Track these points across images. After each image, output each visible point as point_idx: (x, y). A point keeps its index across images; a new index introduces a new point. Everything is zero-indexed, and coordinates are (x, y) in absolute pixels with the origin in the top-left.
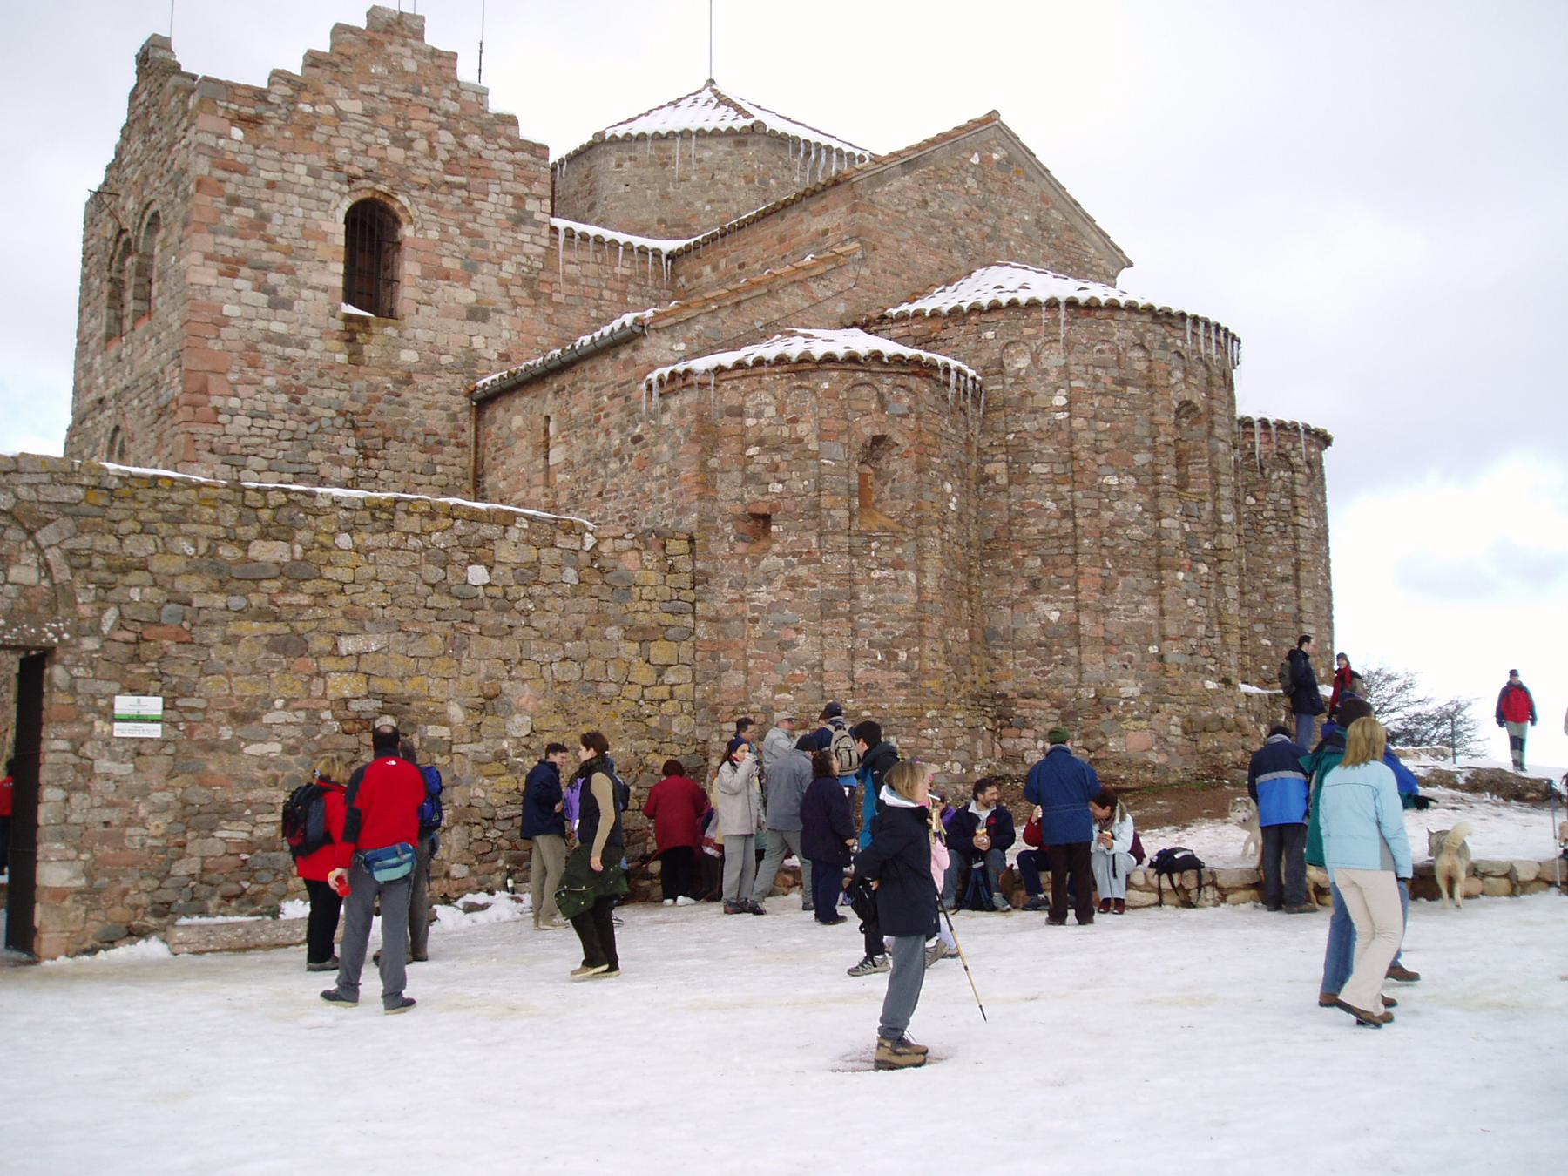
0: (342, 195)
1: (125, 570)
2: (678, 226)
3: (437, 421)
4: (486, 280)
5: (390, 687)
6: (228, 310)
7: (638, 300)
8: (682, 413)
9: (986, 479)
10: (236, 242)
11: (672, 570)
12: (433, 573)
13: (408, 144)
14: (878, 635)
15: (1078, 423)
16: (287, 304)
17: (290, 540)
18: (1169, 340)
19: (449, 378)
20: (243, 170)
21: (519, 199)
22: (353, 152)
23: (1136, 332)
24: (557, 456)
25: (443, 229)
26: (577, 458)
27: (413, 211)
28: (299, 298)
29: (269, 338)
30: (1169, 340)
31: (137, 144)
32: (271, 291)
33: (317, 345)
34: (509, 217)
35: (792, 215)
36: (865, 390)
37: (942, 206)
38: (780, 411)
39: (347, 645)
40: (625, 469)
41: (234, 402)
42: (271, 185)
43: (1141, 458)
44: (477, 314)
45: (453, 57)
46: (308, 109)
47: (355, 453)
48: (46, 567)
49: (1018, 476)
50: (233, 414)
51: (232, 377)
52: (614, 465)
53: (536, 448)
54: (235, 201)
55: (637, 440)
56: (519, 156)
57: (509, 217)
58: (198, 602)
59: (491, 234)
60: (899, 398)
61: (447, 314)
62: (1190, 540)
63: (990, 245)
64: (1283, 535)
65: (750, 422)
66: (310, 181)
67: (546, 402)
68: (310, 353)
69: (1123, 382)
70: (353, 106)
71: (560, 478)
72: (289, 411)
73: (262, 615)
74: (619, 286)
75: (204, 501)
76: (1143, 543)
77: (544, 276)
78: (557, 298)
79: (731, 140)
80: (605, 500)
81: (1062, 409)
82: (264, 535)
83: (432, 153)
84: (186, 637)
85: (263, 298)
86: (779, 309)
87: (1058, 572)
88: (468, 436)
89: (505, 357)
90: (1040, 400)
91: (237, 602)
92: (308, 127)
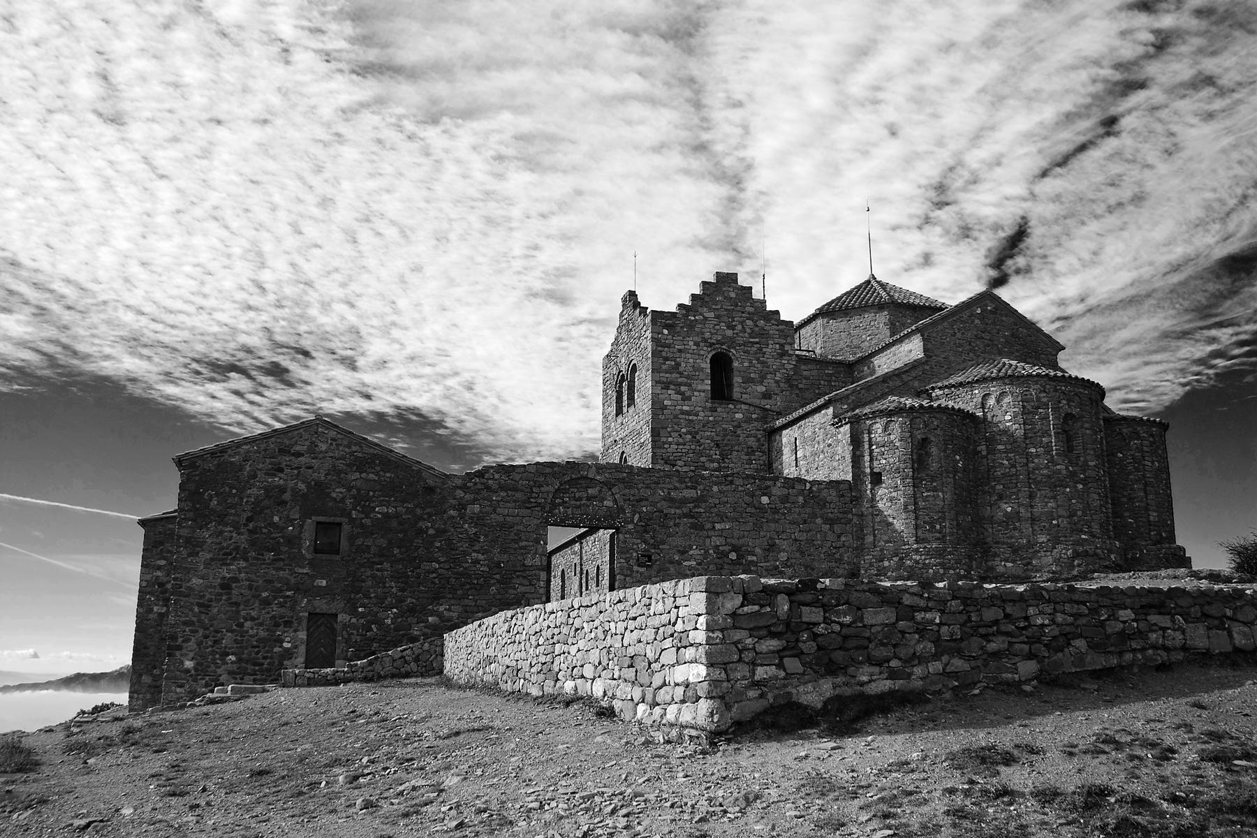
1: (641, 500)
3: (752, 442)
4: (769, 380)
5: (733, 541)
6: (666, 402)
11: (842, 496)
12: (747, 499)
14: (927, 518)
16: (689, 399)
20: (669, 346)
21: (782, 346)
24: (800, 454)
29: (683, 412)
31: (624, 335)
32: (682, 394)
33: (702, 414)
39: (718, 526)
41: (670, 439)
42: (680, 351)
44: (767, 396)
48: (615, 501)
49: (991, 451)
50: (670, 444)
54: (666, 359)
55: (829, 445)
59: (770, 361)
64: (1137, 470)
68: (940, 787)
73: (685, 516)
76: (1049, 476)
85: (680, 397)
92: (691, 326)
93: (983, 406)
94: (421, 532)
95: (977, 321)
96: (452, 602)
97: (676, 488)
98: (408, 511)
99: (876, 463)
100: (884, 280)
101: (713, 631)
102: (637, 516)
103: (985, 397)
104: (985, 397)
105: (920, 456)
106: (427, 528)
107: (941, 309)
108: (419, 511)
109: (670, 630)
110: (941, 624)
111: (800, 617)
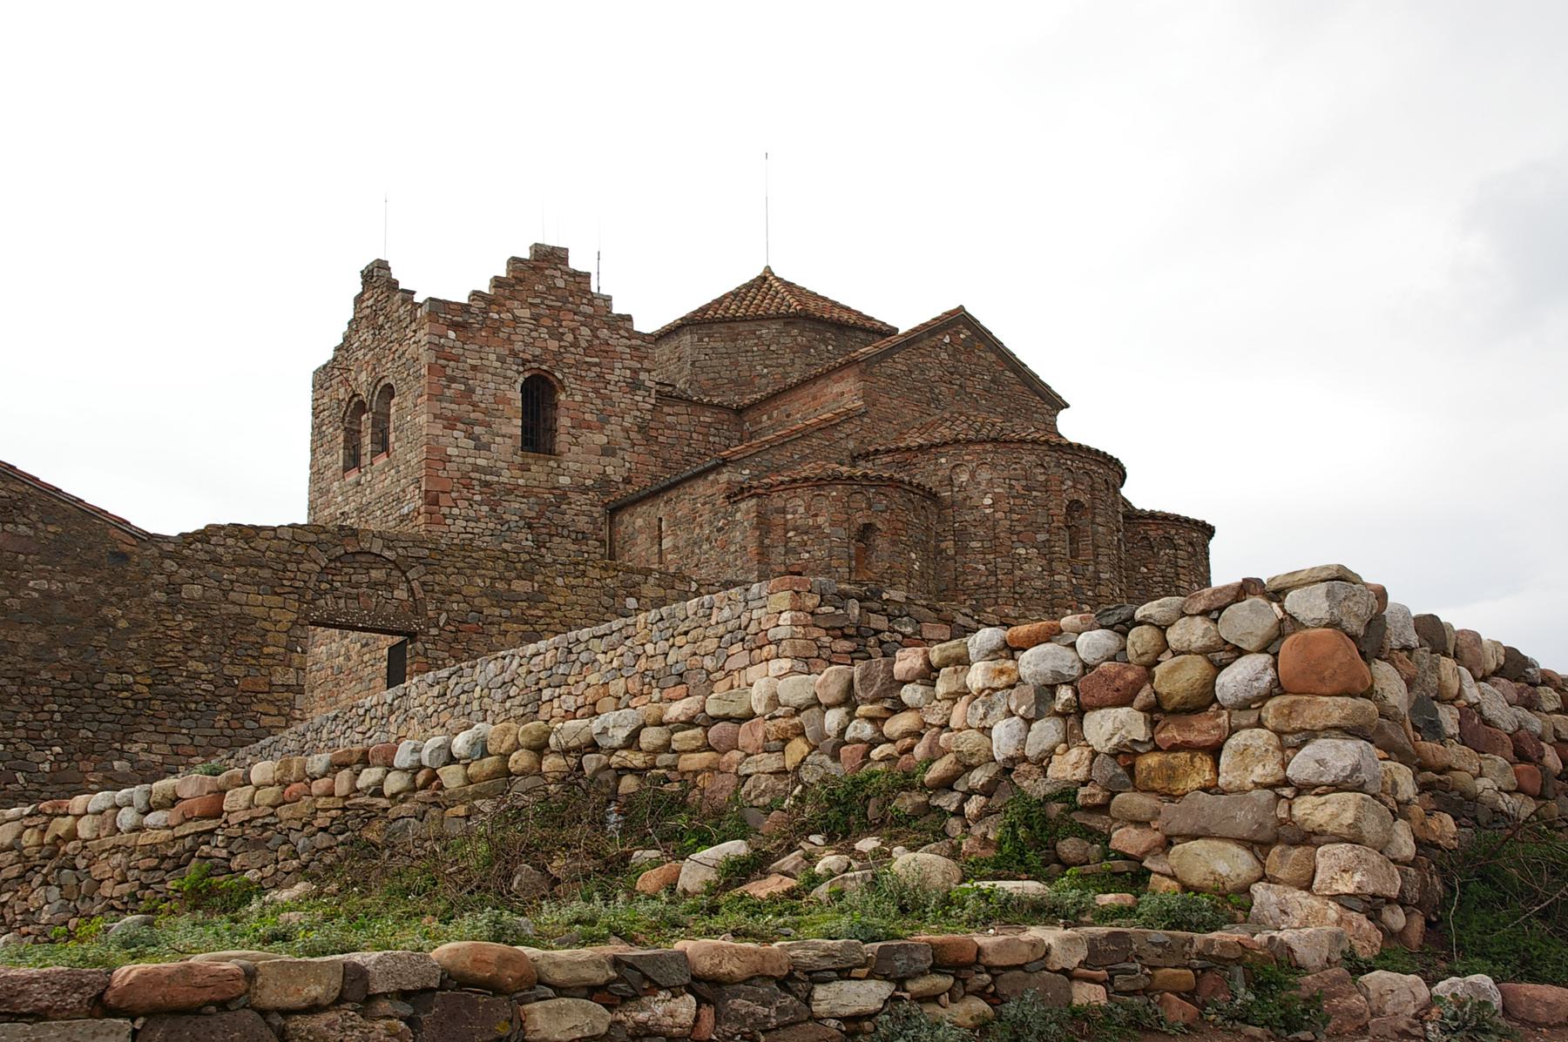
3: (582, 523)
4: (614, 427)
6: (450, 451)
8: (748, 513)
9: (941, 551)
10: (453, 406)
12: (606, 600)
13: (560, 337)
15: (999, 515)
17: (532, 580)
21: (635, 371)
22: (526, 345)
29: (476, 468)
31: (367, 335)
32: (476, 438)
33: (506, 473)
35: (820, 383)
36: (859, 496)
38: (807, 509)
40: (712, 548)
41: (455, 511)
42: (474, 368)
43: (1041, 537)
44: (608, 451)
45: (588, 275)
48: (411, 591)
49: (962, 549)
51: (454, 495)
53: (653, 539)
54: (452, 380)
55: (720, 530)
56: (634, 342)
58: (486, 612)
59: (616, 396)
60: (880, 502)
61: (589, 452)
62: (1076, 590)
65: (789, 516)
67: (661, 509)
69: (1028, 489)
70: (525, 313)
74: (704, 430)
75: (488, 558)
77: (652, 424)
78: (661, 439)
79: (781, 322)
81: (990, 506)
82: (519, 577)
83: (575, 344)
88: (605, 533)
89: (627, 481)
91: (505, 613)
94: (104, 624)
95: (944, 355)
96: (155, 737)
98: (84, 588)
102: (444, 616)
106: (116, 618)
108: (102, 591)
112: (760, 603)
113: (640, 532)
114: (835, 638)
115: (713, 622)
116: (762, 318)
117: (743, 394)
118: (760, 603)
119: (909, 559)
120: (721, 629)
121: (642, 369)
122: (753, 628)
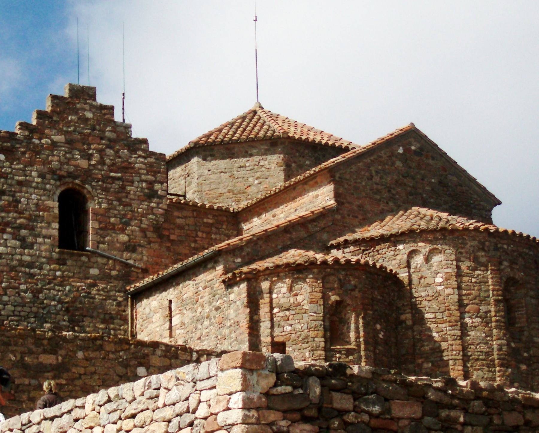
0: (57, 187)
2: (240, 194)
4: (133, 227)
7: (218, 237)
18: (499, 246)
19: (116, 283)
21: (151, 184)
23: (479, 242)
25: (109, 202)
26: (187, 321)
27: (94, 192)
28: (36, 243)
29: (22, 263)
30: (499, 246)
32: (23, 240)
34: (145, 195)
37: (381, 178)
42: (20, 183)
44: (130, 247)
45: (112, 108)
46: (37, 141)
47: (68, 324)
52: (206, 323)
53: (164, 317)
55: (218, 309)
57: (145, 195)
63: (411, 197)
66: (40, 180)
67: (171, 293)
70: (59, 138)
71: (178, 332)
72: (34, 303)
74: (207, 229)
77: (166, 226)
78: (172, 237)
80: (202, 341)
81: (440, 284)
82: (45, 352)
84: (12, 398)
86: (291, 239)
87: (440, 370)
90: (429, 280)
93: (408, 266)
97: (30, 353)
99: (277, 331)
100: (274, 111)
101: (249, 409)
103: (411, 254)
104: (411, 254)
105: (332, 322)
107: (347, 149)
109: (188, 418)
110: (464, 424)
111: (331, 403)
112: (208, 383)
113: (155, 312)
114: (294, 422)
115: (160, 403)
116: (253, 140)
117: (239, 201)
118: (208, 383)
119: (375, 330)
120: (168, 412)
121: (155, 182)
122: (202, 411)
